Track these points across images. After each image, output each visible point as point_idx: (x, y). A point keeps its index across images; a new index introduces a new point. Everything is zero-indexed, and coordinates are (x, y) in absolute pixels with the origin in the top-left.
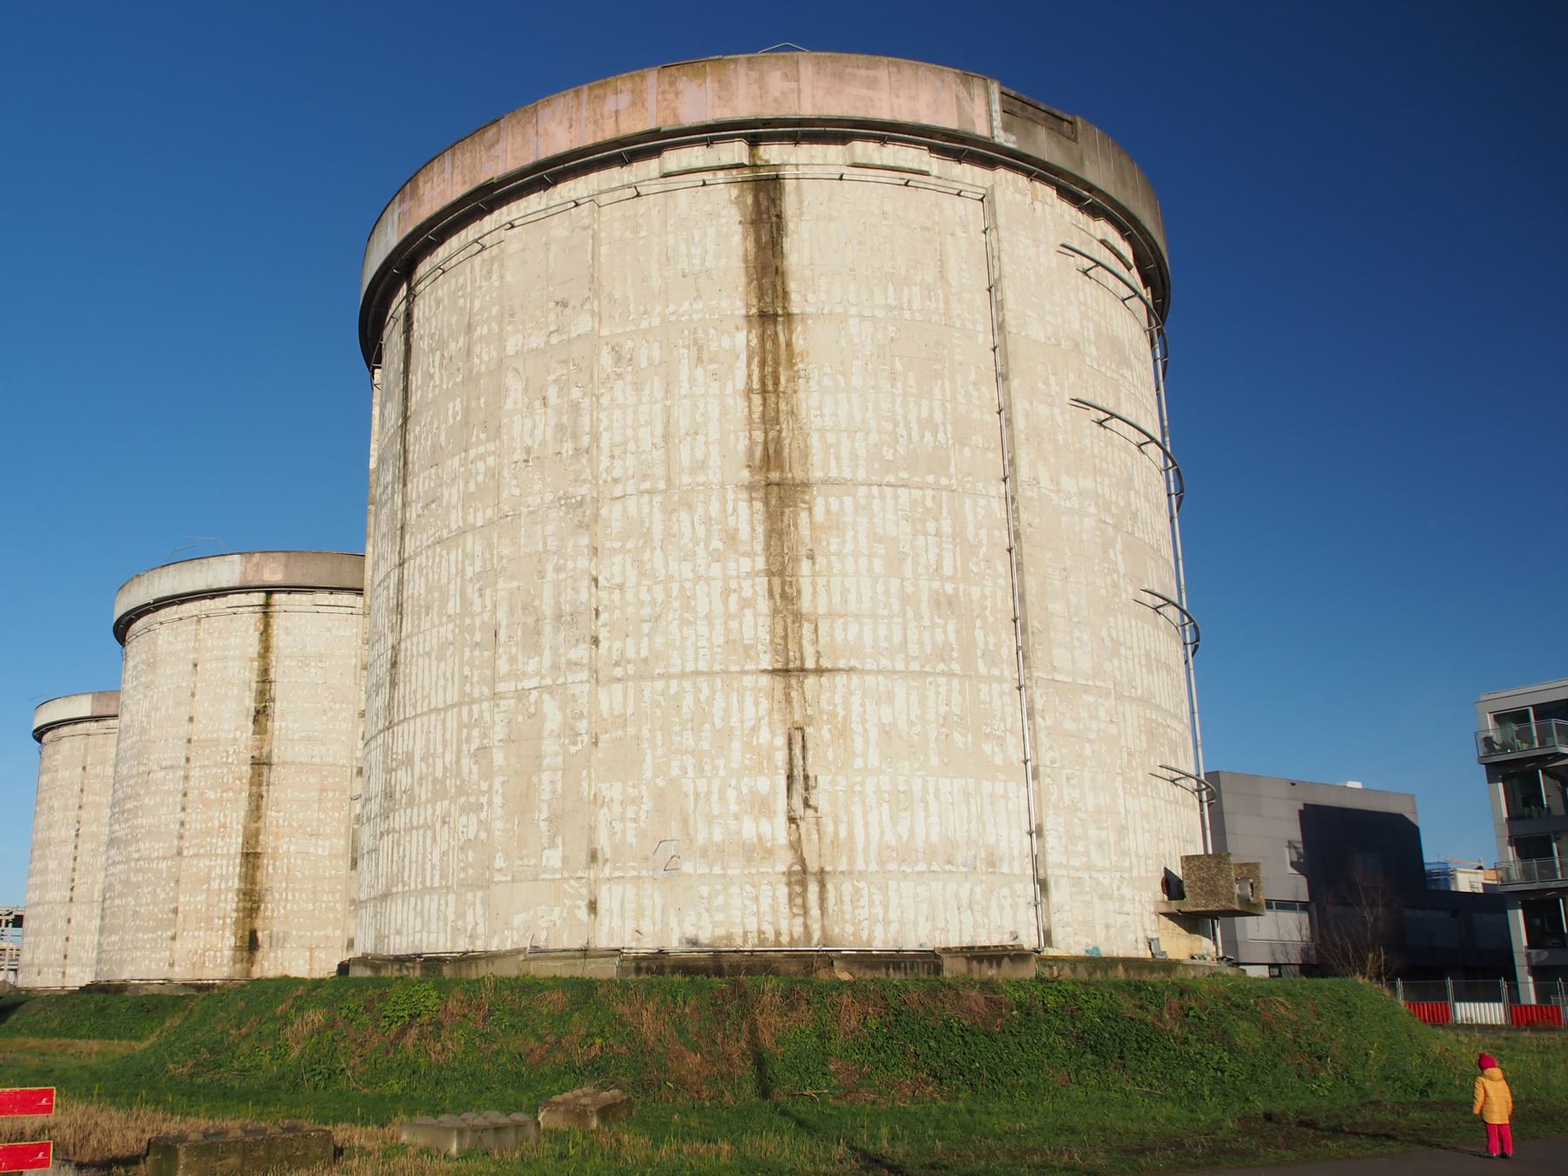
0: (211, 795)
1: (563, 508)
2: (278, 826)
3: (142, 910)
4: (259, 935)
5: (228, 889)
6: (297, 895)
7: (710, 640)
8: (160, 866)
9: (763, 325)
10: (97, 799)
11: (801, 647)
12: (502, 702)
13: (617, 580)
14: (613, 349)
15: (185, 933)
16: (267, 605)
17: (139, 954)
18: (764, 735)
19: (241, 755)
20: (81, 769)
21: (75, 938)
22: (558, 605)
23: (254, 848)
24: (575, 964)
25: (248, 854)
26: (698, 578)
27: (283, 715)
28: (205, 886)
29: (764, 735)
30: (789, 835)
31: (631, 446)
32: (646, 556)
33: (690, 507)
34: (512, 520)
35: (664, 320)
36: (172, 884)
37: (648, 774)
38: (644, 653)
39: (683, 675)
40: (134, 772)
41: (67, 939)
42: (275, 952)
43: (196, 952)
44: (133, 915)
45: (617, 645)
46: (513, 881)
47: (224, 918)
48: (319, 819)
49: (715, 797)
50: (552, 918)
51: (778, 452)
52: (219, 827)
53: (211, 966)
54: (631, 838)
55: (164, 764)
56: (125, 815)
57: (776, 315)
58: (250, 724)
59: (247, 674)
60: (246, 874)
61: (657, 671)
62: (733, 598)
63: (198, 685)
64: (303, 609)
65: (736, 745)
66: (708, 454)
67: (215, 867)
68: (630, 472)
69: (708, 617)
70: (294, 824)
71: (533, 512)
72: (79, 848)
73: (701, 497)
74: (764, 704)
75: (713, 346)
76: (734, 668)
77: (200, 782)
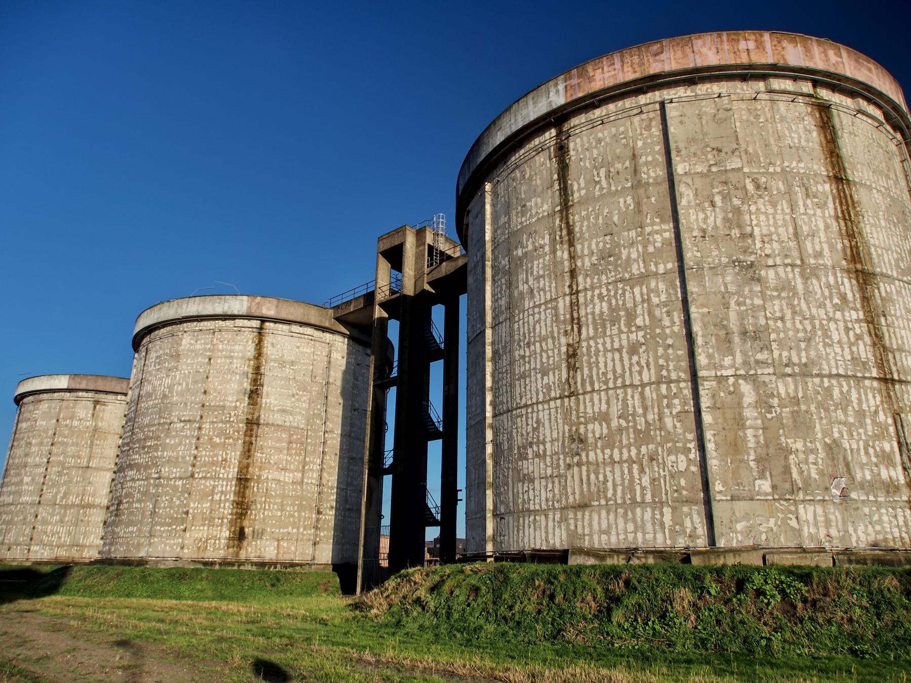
0: (217, 440)
1: (738, 268)
2: (261, 462)
3: (161, 512)
4: (246, 530)
5: (226, 500)
6: (271, 506)
7: (843, 356)
8: (177, 483)
9: (837, 183)
10: (65, 440)
11: (890, 366)
12: (705, 383)
13: (778, 314)
14: (753, 180)
15: (193, 528)
16: (261, 328)
17: (156, 540)
18: (881, 417)
19: (240, 417)
20: (55, 421)
21: (40, 527)
22: (742, 325)
23: (246, 475)
24: (806, 557)
25: (241, 479)
26: (830, 319)
27: (268, 395)
28: (210, 498)
29: (881, 417)
30: (905, 478)
31: (775, 237)
32: (796, 302)
33: (818, 278)
34: (697, 271)
35: (783, 170)
36: (186, 495)
37: (819, 435)
38: (804, 360)
39: (830, 376)
40: (156, 422)
41: (34, 528)
42: (256, 541)
43: (201, 540)
44: (151, 514)
45: (785, 354)
46: (732, 500)
47: (222, 519)
48: (287, 460)
49: (862, 452)
50: (769, 526)
51: (858, 254)
52: (222, 461)
53: (212, 549)
54: (814, 475)
55: (183, 419)
56: (146, 449)
57: (842, 179)
58: (246, 399)
59: (246, 368)
60: (239, 492)
61: (814, 372)
62: (851, 333)
63: (211, 372)
64: (284, 333)
65: (868, 421)
66: (822, 249)
67: (218, 486)
68: (777, 252)
69: (839, 342)
70: (272, 462)
71: (714, 268)
72: (49, 470)
73: (823, 272)
74: (878, 398)
75: (814, 189)
76: (859, 375)
77: (210, 432)
